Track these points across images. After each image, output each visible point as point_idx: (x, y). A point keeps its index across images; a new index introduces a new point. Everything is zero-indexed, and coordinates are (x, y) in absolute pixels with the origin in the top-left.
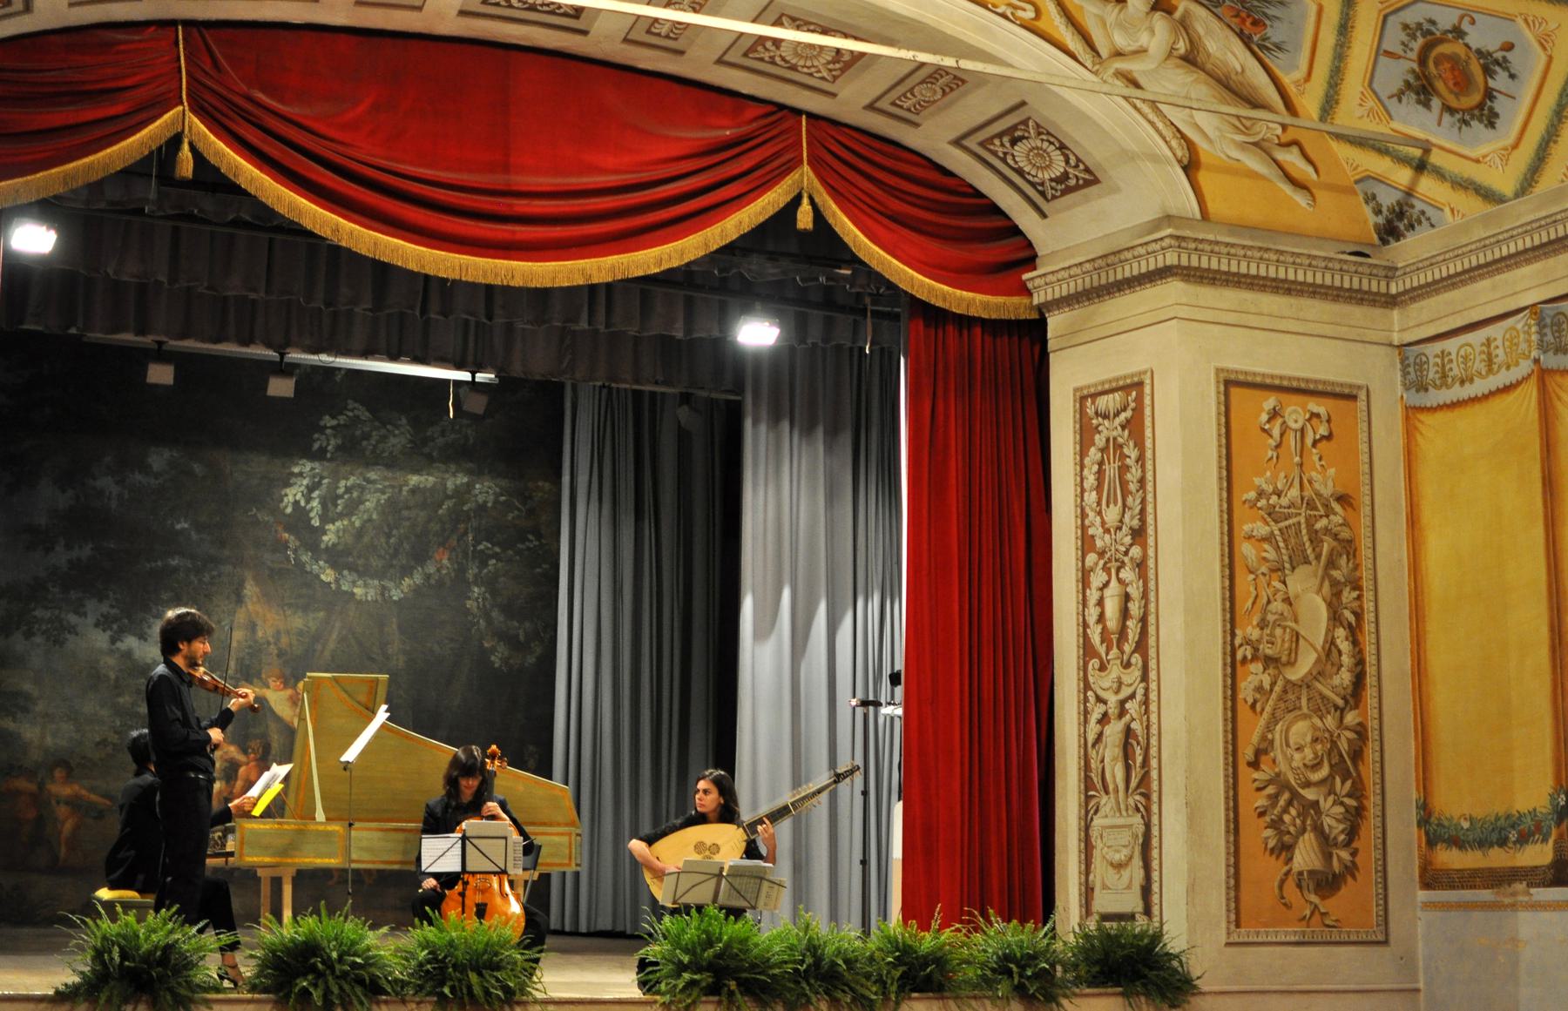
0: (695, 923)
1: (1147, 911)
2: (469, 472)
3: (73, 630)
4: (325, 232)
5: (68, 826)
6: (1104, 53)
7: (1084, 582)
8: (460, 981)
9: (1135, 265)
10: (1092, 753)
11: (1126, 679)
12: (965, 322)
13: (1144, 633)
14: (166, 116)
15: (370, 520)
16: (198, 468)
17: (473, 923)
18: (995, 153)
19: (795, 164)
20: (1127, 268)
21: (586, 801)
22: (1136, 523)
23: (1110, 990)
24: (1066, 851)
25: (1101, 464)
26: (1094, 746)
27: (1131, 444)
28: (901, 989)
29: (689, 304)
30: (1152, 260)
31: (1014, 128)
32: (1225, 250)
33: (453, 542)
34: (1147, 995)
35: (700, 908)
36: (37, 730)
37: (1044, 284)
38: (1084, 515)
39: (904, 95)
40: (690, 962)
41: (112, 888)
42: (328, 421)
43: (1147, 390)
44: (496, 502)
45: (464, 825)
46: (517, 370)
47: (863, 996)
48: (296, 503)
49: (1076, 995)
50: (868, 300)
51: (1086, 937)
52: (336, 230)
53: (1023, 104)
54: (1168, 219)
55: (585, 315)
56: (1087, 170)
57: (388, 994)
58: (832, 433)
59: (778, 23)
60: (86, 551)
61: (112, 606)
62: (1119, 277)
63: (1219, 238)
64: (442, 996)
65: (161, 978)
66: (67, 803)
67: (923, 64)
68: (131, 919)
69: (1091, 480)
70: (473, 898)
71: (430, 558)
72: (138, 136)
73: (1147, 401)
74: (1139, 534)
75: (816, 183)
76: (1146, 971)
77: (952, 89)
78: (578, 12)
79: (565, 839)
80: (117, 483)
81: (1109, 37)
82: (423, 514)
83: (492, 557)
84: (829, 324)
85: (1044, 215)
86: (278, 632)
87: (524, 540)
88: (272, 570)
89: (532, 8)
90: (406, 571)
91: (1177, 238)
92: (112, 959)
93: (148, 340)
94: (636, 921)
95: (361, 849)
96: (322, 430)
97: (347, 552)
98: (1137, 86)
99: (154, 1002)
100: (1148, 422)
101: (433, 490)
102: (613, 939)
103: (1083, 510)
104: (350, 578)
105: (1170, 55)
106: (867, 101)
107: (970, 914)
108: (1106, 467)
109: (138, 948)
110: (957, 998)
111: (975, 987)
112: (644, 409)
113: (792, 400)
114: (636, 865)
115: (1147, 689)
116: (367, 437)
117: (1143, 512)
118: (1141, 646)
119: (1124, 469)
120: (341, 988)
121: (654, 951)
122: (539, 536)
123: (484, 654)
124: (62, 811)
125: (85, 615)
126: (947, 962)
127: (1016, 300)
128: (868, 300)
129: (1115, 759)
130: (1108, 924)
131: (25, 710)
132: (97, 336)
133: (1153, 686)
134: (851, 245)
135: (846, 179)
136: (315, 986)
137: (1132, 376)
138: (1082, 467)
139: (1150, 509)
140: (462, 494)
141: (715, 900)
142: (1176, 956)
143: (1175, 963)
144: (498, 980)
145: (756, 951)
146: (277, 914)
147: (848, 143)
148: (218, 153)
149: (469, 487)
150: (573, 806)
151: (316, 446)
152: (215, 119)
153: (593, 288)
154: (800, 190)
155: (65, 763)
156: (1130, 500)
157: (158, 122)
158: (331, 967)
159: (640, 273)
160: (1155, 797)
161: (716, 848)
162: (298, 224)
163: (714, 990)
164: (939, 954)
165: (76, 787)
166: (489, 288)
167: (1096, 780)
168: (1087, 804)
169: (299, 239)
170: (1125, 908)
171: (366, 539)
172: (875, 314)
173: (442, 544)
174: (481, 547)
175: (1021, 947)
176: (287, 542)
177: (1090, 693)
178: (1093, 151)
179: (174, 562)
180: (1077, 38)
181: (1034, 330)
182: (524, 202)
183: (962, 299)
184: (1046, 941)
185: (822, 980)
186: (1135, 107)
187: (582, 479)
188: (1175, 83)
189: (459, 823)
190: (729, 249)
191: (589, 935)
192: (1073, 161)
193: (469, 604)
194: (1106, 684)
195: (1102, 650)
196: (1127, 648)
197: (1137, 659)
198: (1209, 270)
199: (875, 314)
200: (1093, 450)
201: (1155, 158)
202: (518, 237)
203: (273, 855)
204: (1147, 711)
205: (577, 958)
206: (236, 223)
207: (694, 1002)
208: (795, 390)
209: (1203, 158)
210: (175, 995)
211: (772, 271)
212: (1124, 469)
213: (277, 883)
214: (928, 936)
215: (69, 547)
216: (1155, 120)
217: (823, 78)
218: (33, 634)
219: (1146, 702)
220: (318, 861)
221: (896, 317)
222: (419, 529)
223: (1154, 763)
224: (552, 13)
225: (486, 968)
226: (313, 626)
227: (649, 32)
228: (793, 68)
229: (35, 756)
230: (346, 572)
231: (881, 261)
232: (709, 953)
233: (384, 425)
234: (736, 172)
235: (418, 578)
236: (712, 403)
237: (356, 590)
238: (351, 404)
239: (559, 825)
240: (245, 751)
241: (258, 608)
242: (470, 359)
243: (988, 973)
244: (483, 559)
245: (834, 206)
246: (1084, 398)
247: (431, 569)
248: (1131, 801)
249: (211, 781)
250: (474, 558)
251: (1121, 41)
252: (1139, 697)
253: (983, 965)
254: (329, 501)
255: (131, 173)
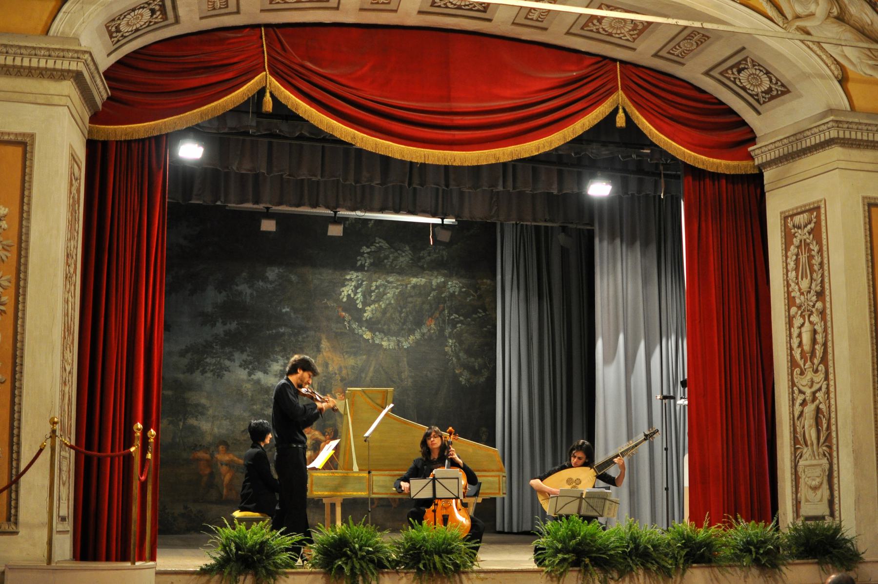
0: (565, 525)
1: (832, 514)
2: (445, 276)
3: (227, 369)
4: (348, 139)
5: (227, 478)
6: (790, 17)
7: (790, 324)
8: (429, 560)
9: (813, 139)
10: (798, 423)
11: (816, 379)
12: (716, 176)
13: (825, 352)
14: (257, 78)
15: (390, 304)
16: (293, 278)
17: (440, 526)
18: (729, 79)
19: (614, 90)
20: (808, 141)
21: (507, 458)
22: (818, 288)
23: (810, 561)
24: (784, 481)
25: (797, 255)
26: (798, 419)
27: (814, 243)
28: (686, 561)
29: (560, 173)
30: (822, 135)
31: (739, 63)
32: (865, 128)
33: (437, 314)
34: (833, 564)
35: (567, 517)
36: (209, 425)
37: (760, 153)
38: (788, 285)
39: (675, 47)
40: (562, 548)
41: (242, 511)
42: (365, 249)
43: (823, 211)
44: (460, 292)
45: (434, 472)
46: (466, 217)
47: (664, 566)
48: (349, 295)
49: (789, 564)
50: (661, 168)
51: (795, 529)
52: (354, 138)
53: (744, 48)
54: (831, 111)
55: (501, 183)
56: (783, 85)
57: (388, 568)
58: (645, 245)
59: (600, 8)
60: (233, 326)
61: (248, 356)
62: (804, 146)
63: (861, 121)
64: (419, 569)
65: (260, 561)
66: (226, 465)
67: (686, 27)
68: (243, 527)
69: (792, 265)
70: (440, 513)
71: (424, 324)
72: (241, 90)
73: (823, 217)
74: (820, 295)
75: (627, 100)
76: (831, 549)
77: (702, 43)
78: (486, 7)
79: (496, 479)
80: (249, 287)
81: (792, 8)
82: (419, 300)
83: (458, 322)
84: (640, 182)
85: (759, 113)
86: (341, 368)
87: (476, 312)
88: (336, 333)
89: (459, 8)
90: (411, 332)
91: (837, 121)
92: (231, 550)
93: (261, 207)
94: (533, 524)
95: (380, 486)
96: (362, 254)
97: (378, 322)
98: (808, 33)
99: (256, 574)
100: (824, 229)
101: (425, 286)
102: (523, 535)
103: (788, 282)
104: (380, 336)
105: (828, 16)
106: (653, 52)
107: (728, 518)
108: (801, 256)
109: (246, 544)
110: (720, 566)
111: (731, 559)
112: (542, 237)
113: (621, 228)
114: (534, 491)
115: (828, 385)
116: (387, 257)
117: (822, 282)
118: (824, 360)
119: (810, 257)
120: (361, 565)
121: (542, 541)
122: (485, 310)
123: (456, 377)
124: (224, 469)
125: (234, 361)
126: (713, 546)
127: (745, 163)
128: (661, 168)
129: (810, 426)
130: (809, 522)
131: (202, 414)
132: (232, 205)
133: (832, 383)
134: (648, 135)
135: (641, 96)
136: (346, 564)
137: (814, 203)
138: (787, 257)
139: (826, 280)
140: (441, 287)
141: (579, 512)
142: (850, 541)
143: (849, 545)
144: (450, 559)
145: (600, 541)
146: (333, 522)
147: (642, 76)
148: (286, 97)
149: (445, 284)
150: (501, 460)
151: (359, 263)
152: (283, 78)
153: (505, 165)
154: (617, 105)
155: (224, 443)
156: (815, 275)
157: (252, 81)
158: (356, 553)
159: (527, 155)
160: (834, 448)
161: (578, 481)
162: (332, 135)
163: (576, 564)
164: (708, 541)
165: (231, 456)
166: (446, 167)
167: (800, 438)
168: (795, 453)
169: (338, 146)
170: (818, 513)
171: (388, 315)
172: (666, 176)
173: (431, 316)
174: (452, 317)
175: (757, 537)
176: (344, 317)
177: (795, 388)
178: (786, 74)
179: (282, 330)
180: (773, 9)
181: (756, 179)
182: (459, 118)
183: (713, 163)
184: (771, 533)
185: (640, 557)
186: (809, 47)
187: (508, 277)
188: (834, 31)
189: (432, 471)
190: (578, 140)
191: (518, 533)
192: (774, 81)
193: (447, 349)
194: (804, 383)
195: (801, 363)
196: (816, 361)
197: (822, 367)
198: (856, 140)
199: (666, 176)
200: (792, 247)
201: (822, 77)
202: (457, 137)
203: (330, 491)
204: (828, 398)
205: (508, 547)
206: (301, 137)
207: (565, 571)
208: (619, 221)
209: (851, 75)
210: (267, 570)
211: (605, 152)
212: (810, 257)
213: (333, 506)
214: (702, 531)
215: (224, 324)
216: (821, 54)
217: (628, 40)
218: (206, 372)
219: (828, 392)
220: (355, 493)
221: (678, 177)
222: (417, 308)
223: (833, 428)
224: (471, 10)
225: (444, 552)
226: (360, 363)
227: (526, 18)
228: (610, 35)
229: (209, 439)
230: (377, 333)
231: (666, 143)
232: (573, 542)
233: (396, 250)
234: (580, 96)
235: (418, 335)
236: (580, 231)
237: (383, 343)
238: (378, 240)
239: (493, 471)
240: (324, 434)
241: (329, 354)
242: (440, 210)
243: (738, 552)
244: (454, 324)
245: (637, 113)
246: (786, 217)
247: (425, 330)
248: (821, 450)
249: (305, 449)
250: (449, 323)
251: (799, 9)
252: (824, 389)
253: (734, 547)
254: (367, 294)
255: (239, 111)
